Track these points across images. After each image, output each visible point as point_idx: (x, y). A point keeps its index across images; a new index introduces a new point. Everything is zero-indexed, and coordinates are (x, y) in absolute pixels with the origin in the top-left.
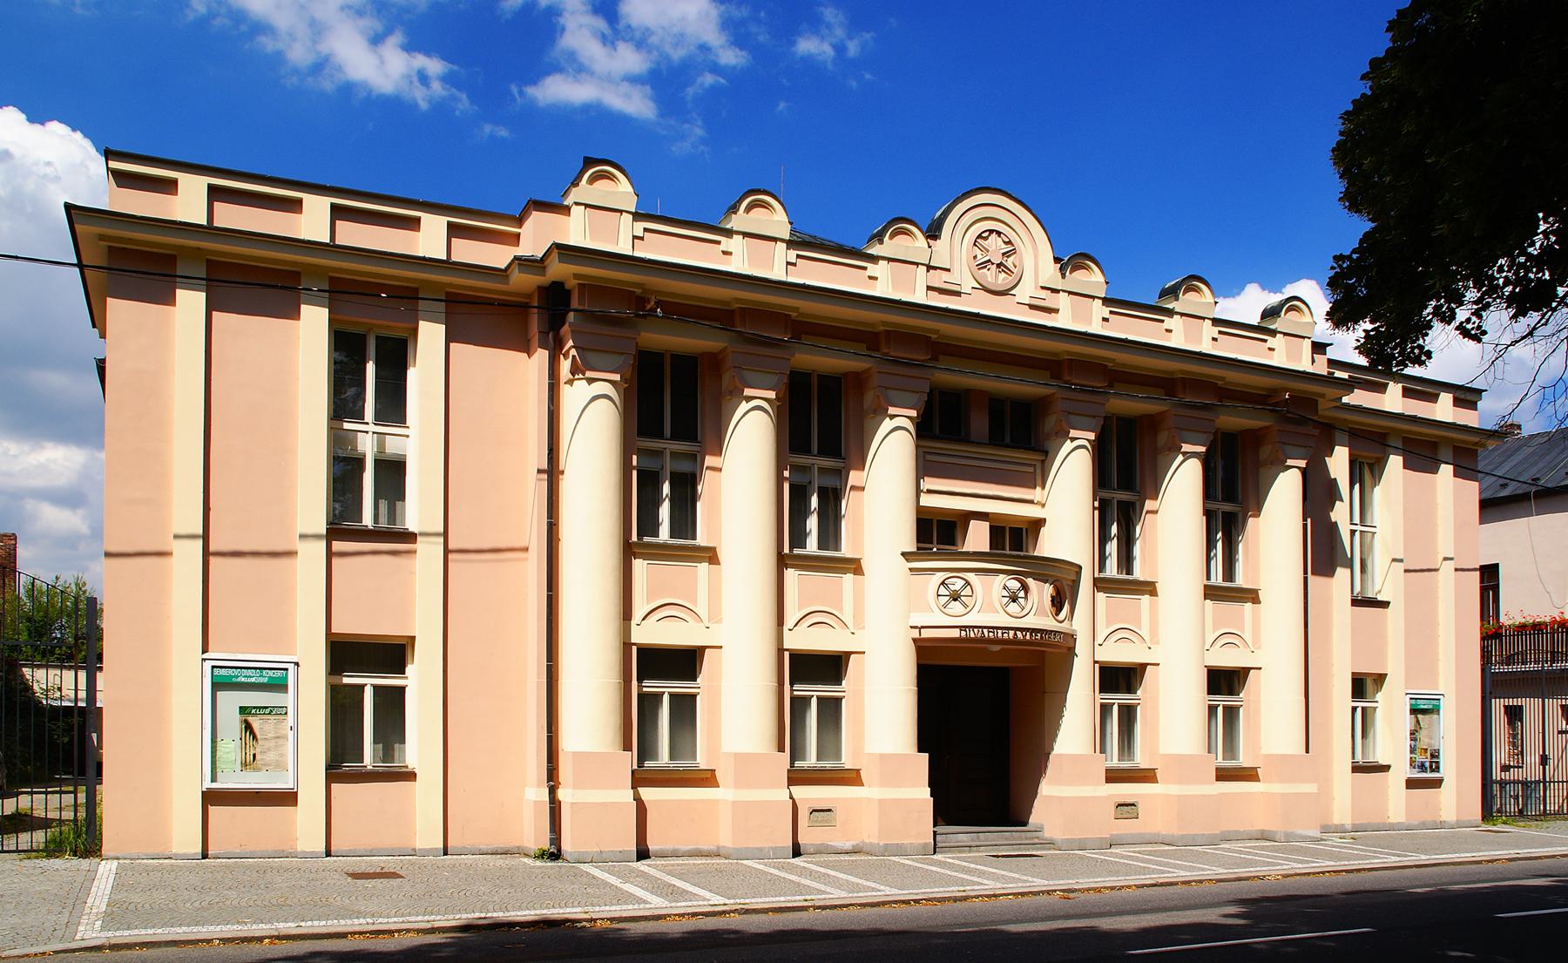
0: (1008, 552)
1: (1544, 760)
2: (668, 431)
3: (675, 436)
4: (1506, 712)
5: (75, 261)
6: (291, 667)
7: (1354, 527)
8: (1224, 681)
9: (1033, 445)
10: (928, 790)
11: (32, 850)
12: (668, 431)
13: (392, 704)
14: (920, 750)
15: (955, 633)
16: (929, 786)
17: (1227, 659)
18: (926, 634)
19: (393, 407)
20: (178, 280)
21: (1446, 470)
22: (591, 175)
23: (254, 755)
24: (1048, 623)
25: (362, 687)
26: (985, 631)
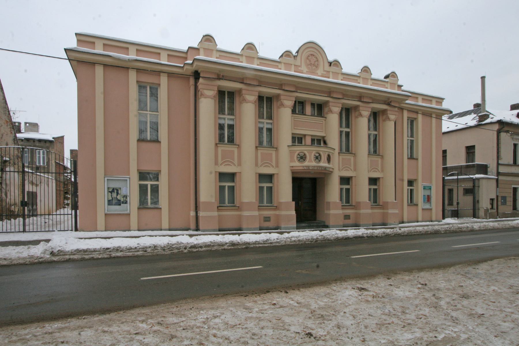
0: (316, 145)
1: (458, 203)
2: (226, 112)
3: (229, 114)
4: (463, 190)
5: (67, 58)
6: (324, 121)
7: (408, 138)
8: (373, 181)
9: (323, 116)
10: (295, 212)
11: (60, 231)
12: (226, 112)
13: (155, 190)
14: (293, 200)
15: (301, 168)
16: (295, 210)
17: (375, 175)
18: (294, 168)
19: (142, 124)
20: (96, 64)
21: (78, 194)
22: (207, 38)
23: (263, 313)
24: (326, 165)
25: (147, 185)
26: (318, 167)
